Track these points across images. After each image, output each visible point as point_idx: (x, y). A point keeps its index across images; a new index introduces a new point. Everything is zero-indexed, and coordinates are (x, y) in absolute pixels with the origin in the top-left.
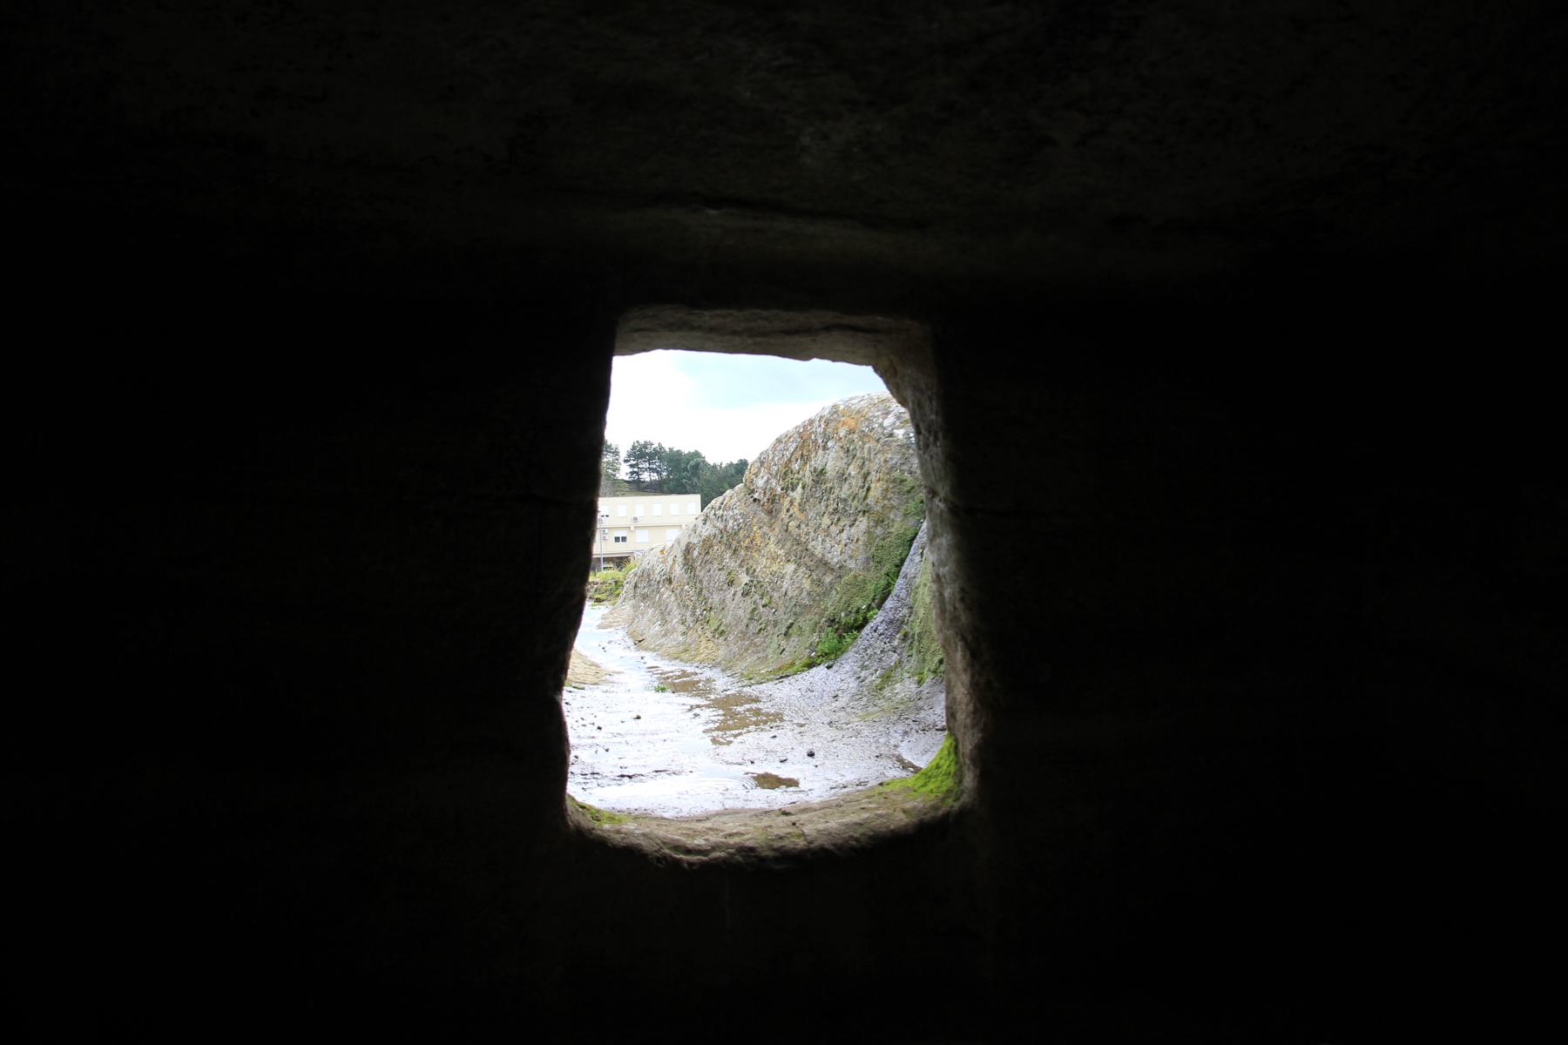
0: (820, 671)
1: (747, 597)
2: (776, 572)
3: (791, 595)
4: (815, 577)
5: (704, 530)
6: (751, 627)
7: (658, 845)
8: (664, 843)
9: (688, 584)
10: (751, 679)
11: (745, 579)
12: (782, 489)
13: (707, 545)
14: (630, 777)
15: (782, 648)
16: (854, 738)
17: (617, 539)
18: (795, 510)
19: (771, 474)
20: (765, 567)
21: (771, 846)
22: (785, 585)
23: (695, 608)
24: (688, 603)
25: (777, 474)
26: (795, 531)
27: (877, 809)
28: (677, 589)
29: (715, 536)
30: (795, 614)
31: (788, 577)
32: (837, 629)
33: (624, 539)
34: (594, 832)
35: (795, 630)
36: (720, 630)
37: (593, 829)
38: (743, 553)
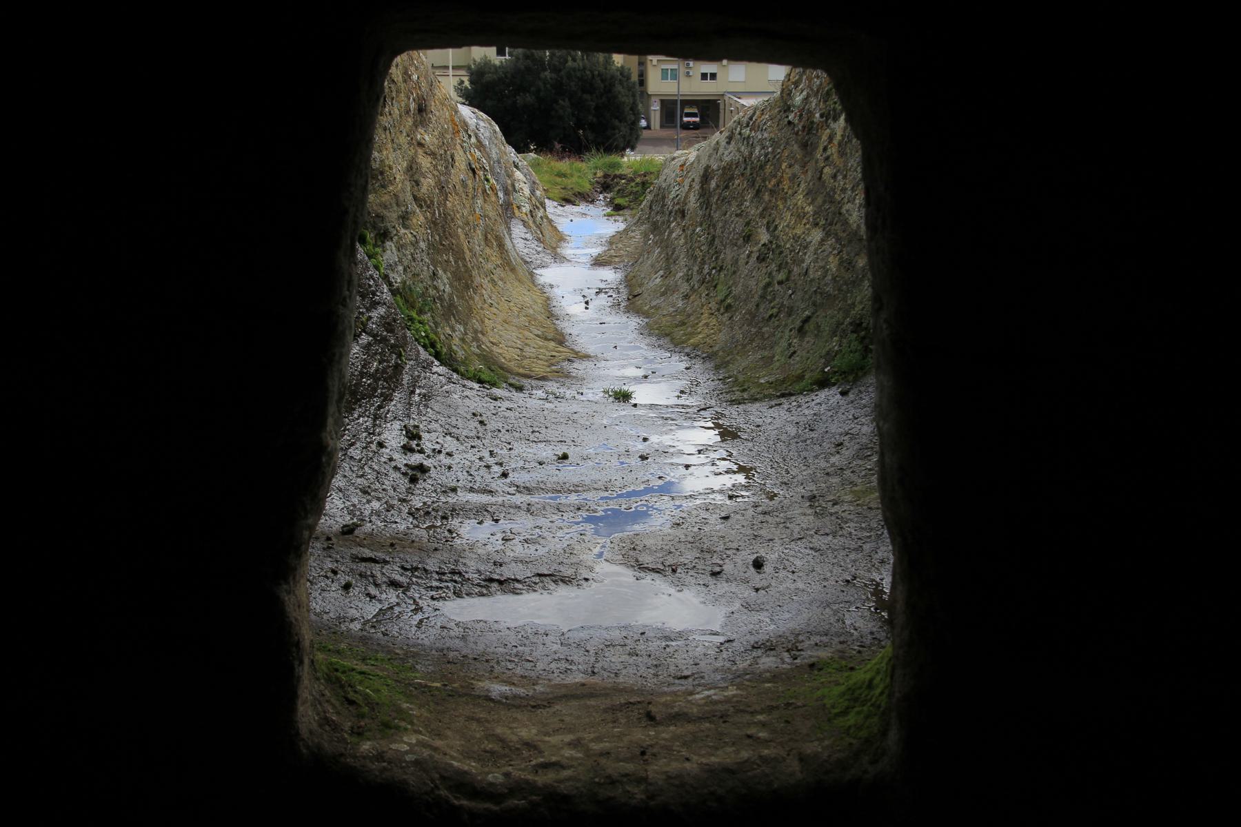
0: (829, 396)
1: (764, 264)
2: (799, 237)
3: (812, 277)
4: (845, 256)
5: (726, 153)
6: (762, 307)
7: (433, 781)
8: (443, 778)
9: (701, 226)
10: (744, 390)
11: (764, 237)
12: (822, 116)
13: (728, 173)
14: (501, 582)
15: (792, 349)
16: (830, 538)
17: (704, 76)
18: (833, 150)
19: (812, 90)
20: (787, 226)
21: (670, 714)
22: (808, 259)
23: (703, 262)
24: (698, 252)
25: (818, 91)
26: (830, 183)
27: (766, 742)
28: (688, 228)
29: (737, 164)
30: (814, 304)
31: (812, 249)
32: (864, 338)
33: (713, 76)
34: (342, 759)
35: (812, 327)
36: (726, 304)
37: (342, 755)
38: (766, 197)
